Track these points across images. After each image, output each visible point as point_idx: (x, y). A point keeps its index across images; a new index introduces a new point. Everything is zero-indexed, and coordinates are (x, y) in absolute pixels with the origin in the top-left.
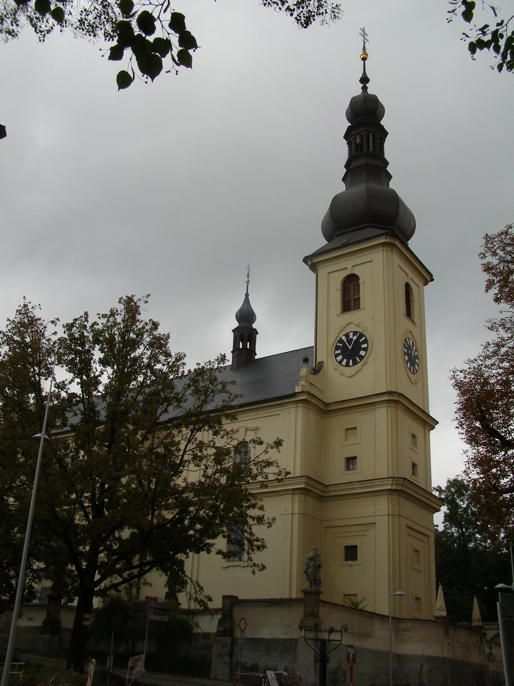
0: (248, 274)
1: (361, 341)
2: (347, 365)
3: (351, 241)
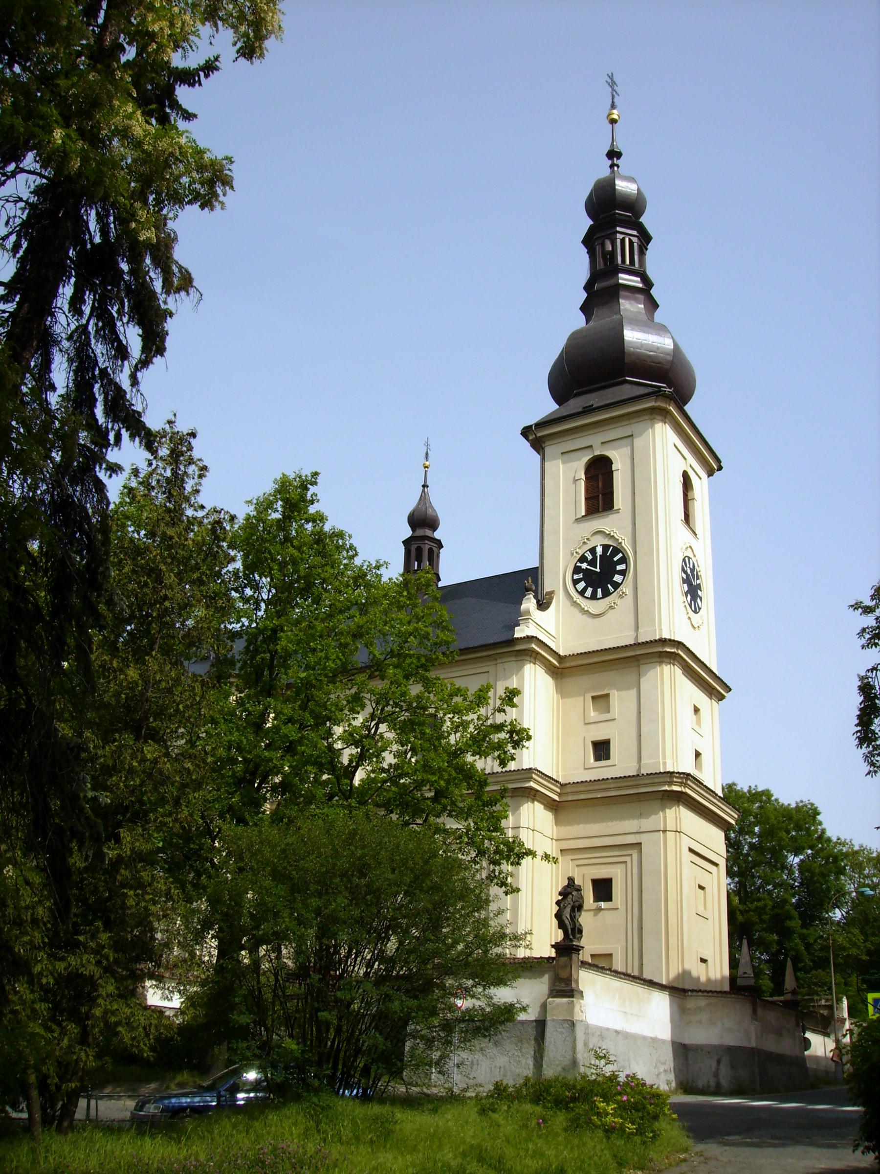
0: (427, 454)
1: (615, 559)
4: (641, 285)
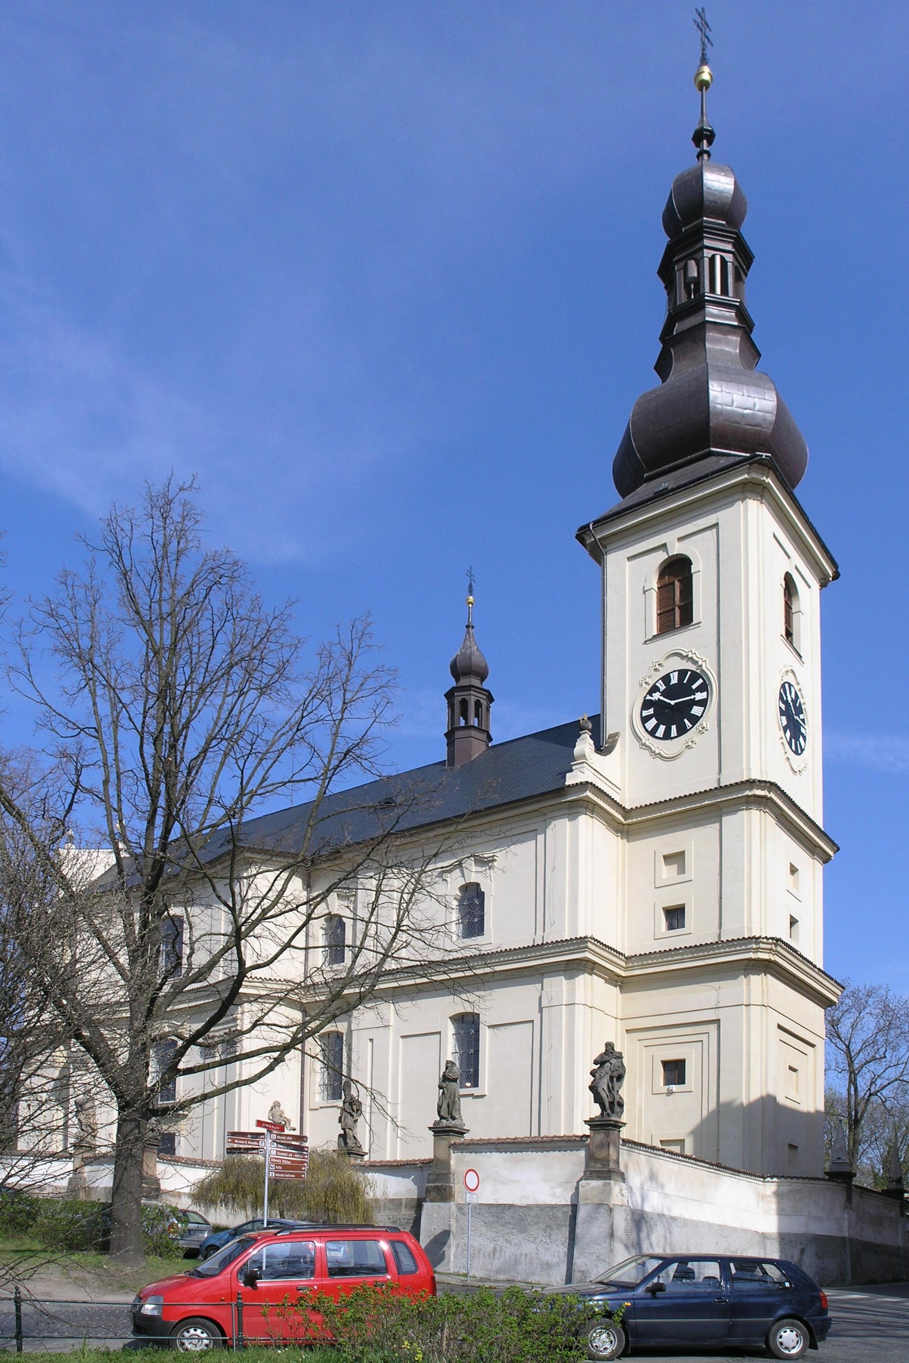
0: (471, 586)
4: (736, 323)
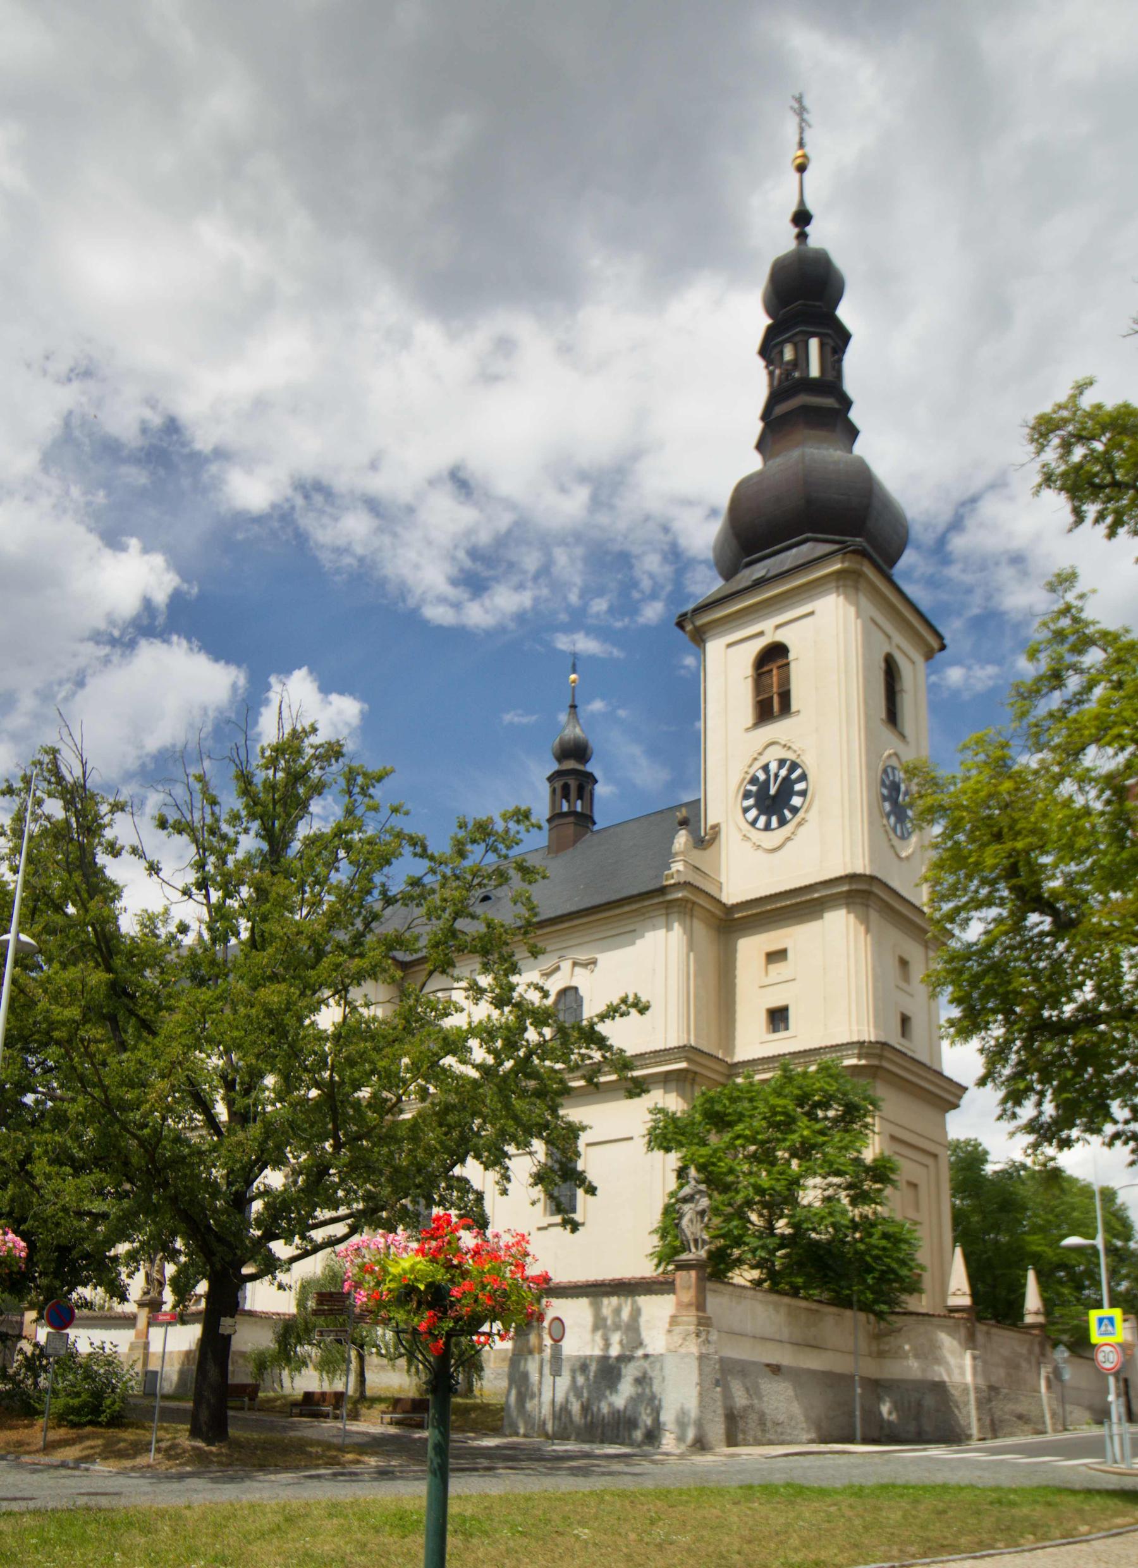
0: (801, 139)
2: (767, 827)
3: (770, 574)
